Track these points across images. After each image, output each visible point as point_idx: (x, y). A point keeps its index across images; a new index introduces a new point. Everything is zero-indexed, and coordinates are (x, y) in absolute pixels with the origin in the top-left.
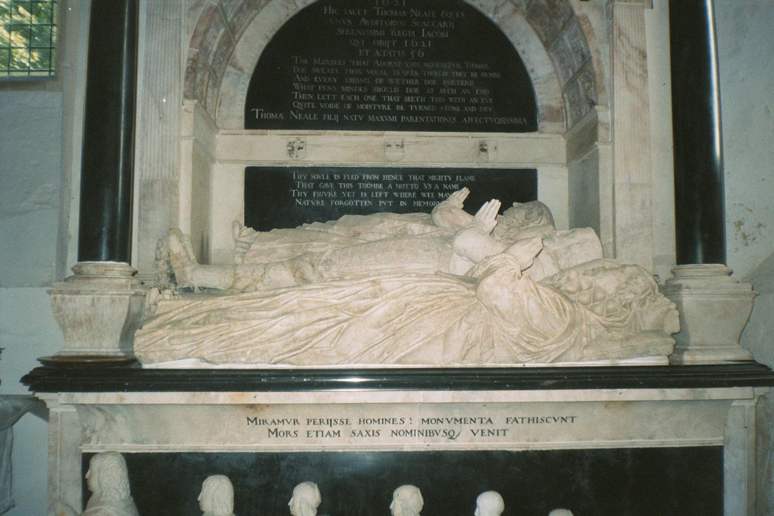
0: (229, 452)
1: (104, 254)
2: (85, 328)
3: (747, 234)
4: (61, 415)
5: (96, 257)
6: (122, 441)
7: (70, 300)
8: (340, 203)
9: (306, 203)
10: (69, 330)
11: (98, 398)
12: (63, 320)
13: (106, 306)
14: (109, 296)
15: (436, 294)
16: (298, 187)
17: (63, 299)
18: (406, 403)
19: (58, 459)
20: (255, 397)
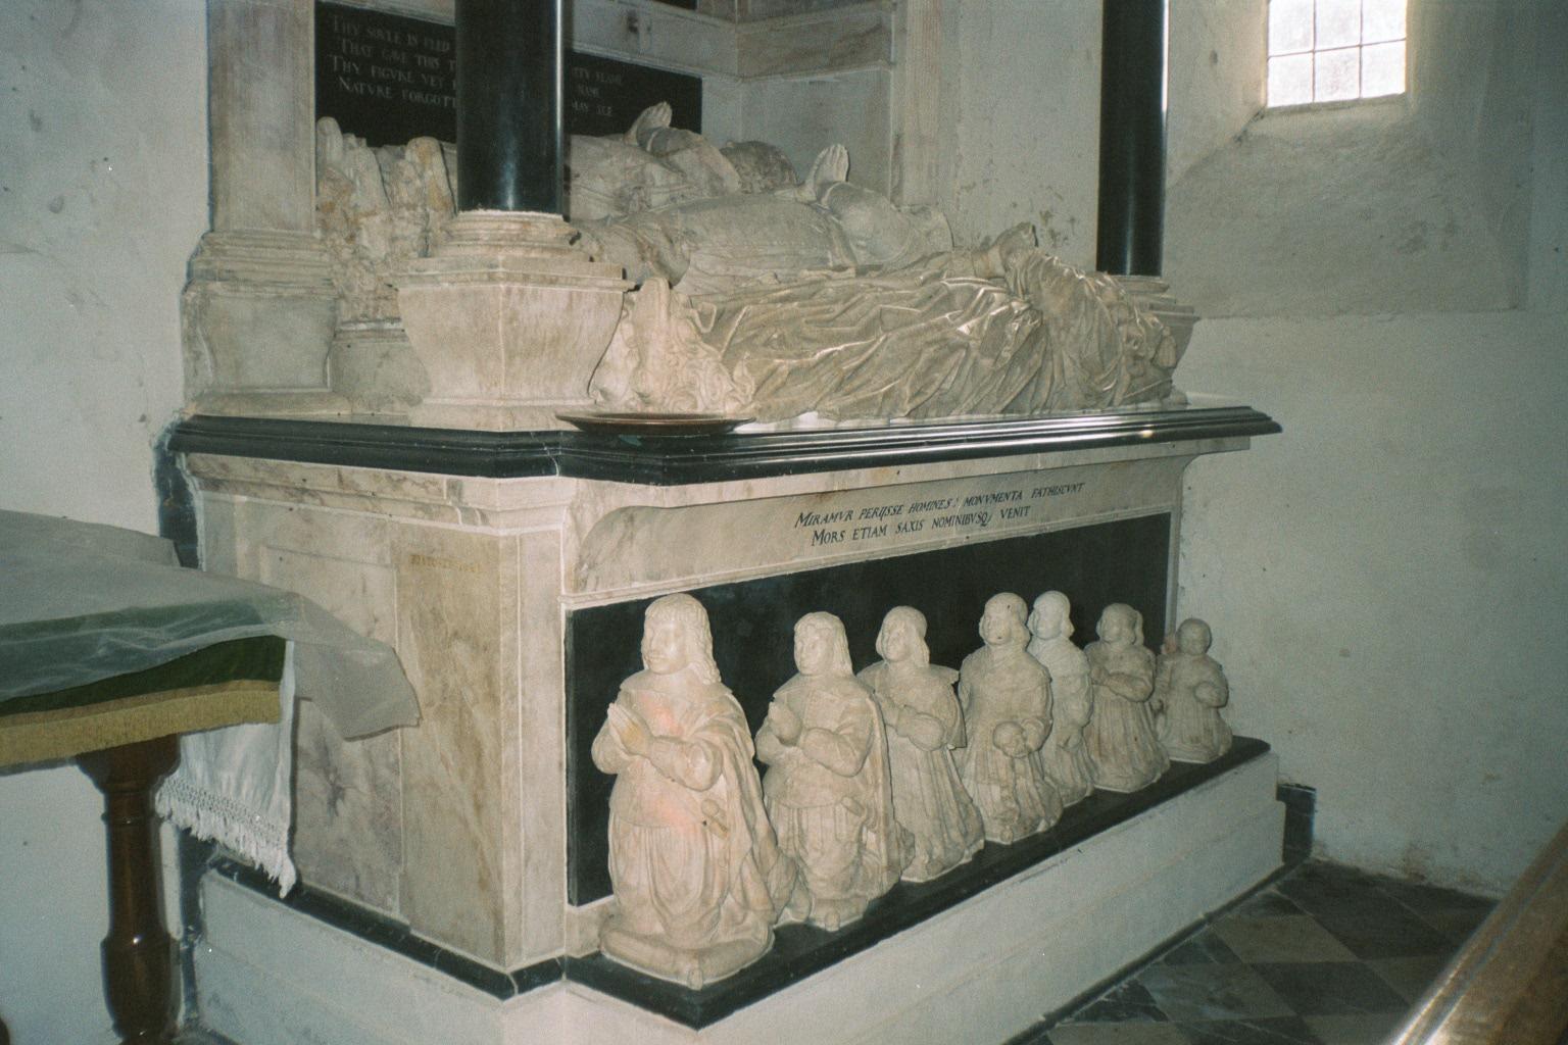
0: (763, 577)
1: (510, 202)
2: (545, 359)
3: (1056, 230)
4: (521, 540)
5: (496, 202)
6: (632, 579)
7: (535, 295)
8: (419, 97)
9: (359, 88)
10: (518, 360)
11: (720, 492)
12: (516, 338)
13: (589, 311)
14: (597, 290)
15: (855, 303)
16: (344, 50)
17: (522, 292)
18: (1131, 461)
19: (519, 632)
20: (898, 473)
